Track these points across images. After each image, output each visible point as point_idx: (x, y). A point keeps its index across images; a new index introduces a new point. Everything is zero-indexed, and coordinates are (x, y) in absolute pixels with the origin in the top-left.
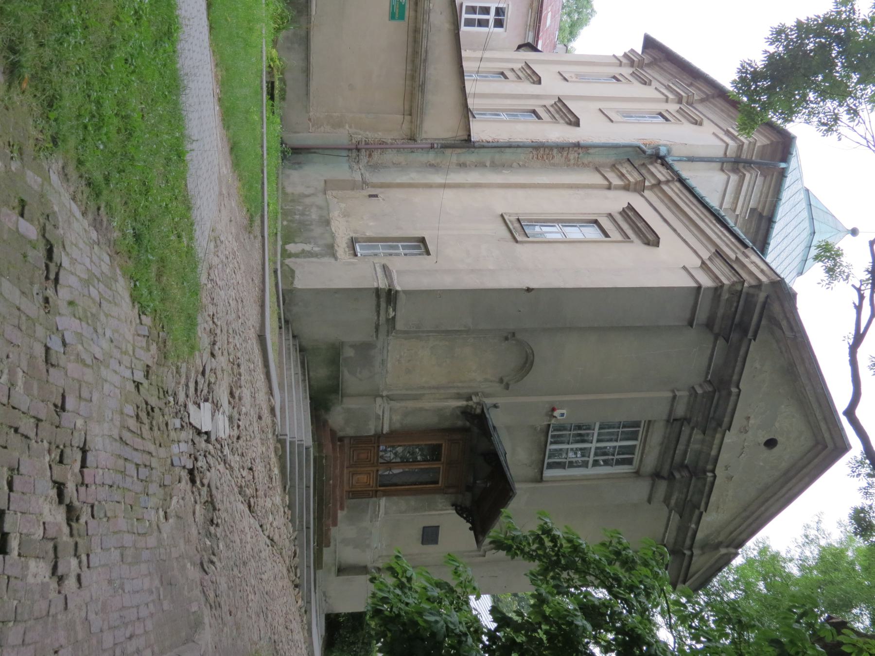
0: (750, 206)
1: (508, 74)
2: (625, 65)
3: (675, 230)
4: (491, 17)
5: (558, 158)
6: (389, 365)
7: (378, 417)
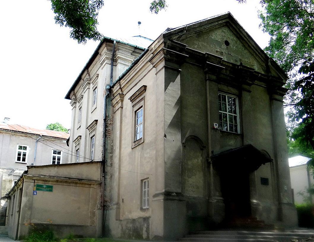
0: (130, 55)
1: (77, 149)
2: (76, 105)
3: (140, 80)
4: (57, 155)
5: (110, 128)
6: (196, 196)
7: (218, 201)
